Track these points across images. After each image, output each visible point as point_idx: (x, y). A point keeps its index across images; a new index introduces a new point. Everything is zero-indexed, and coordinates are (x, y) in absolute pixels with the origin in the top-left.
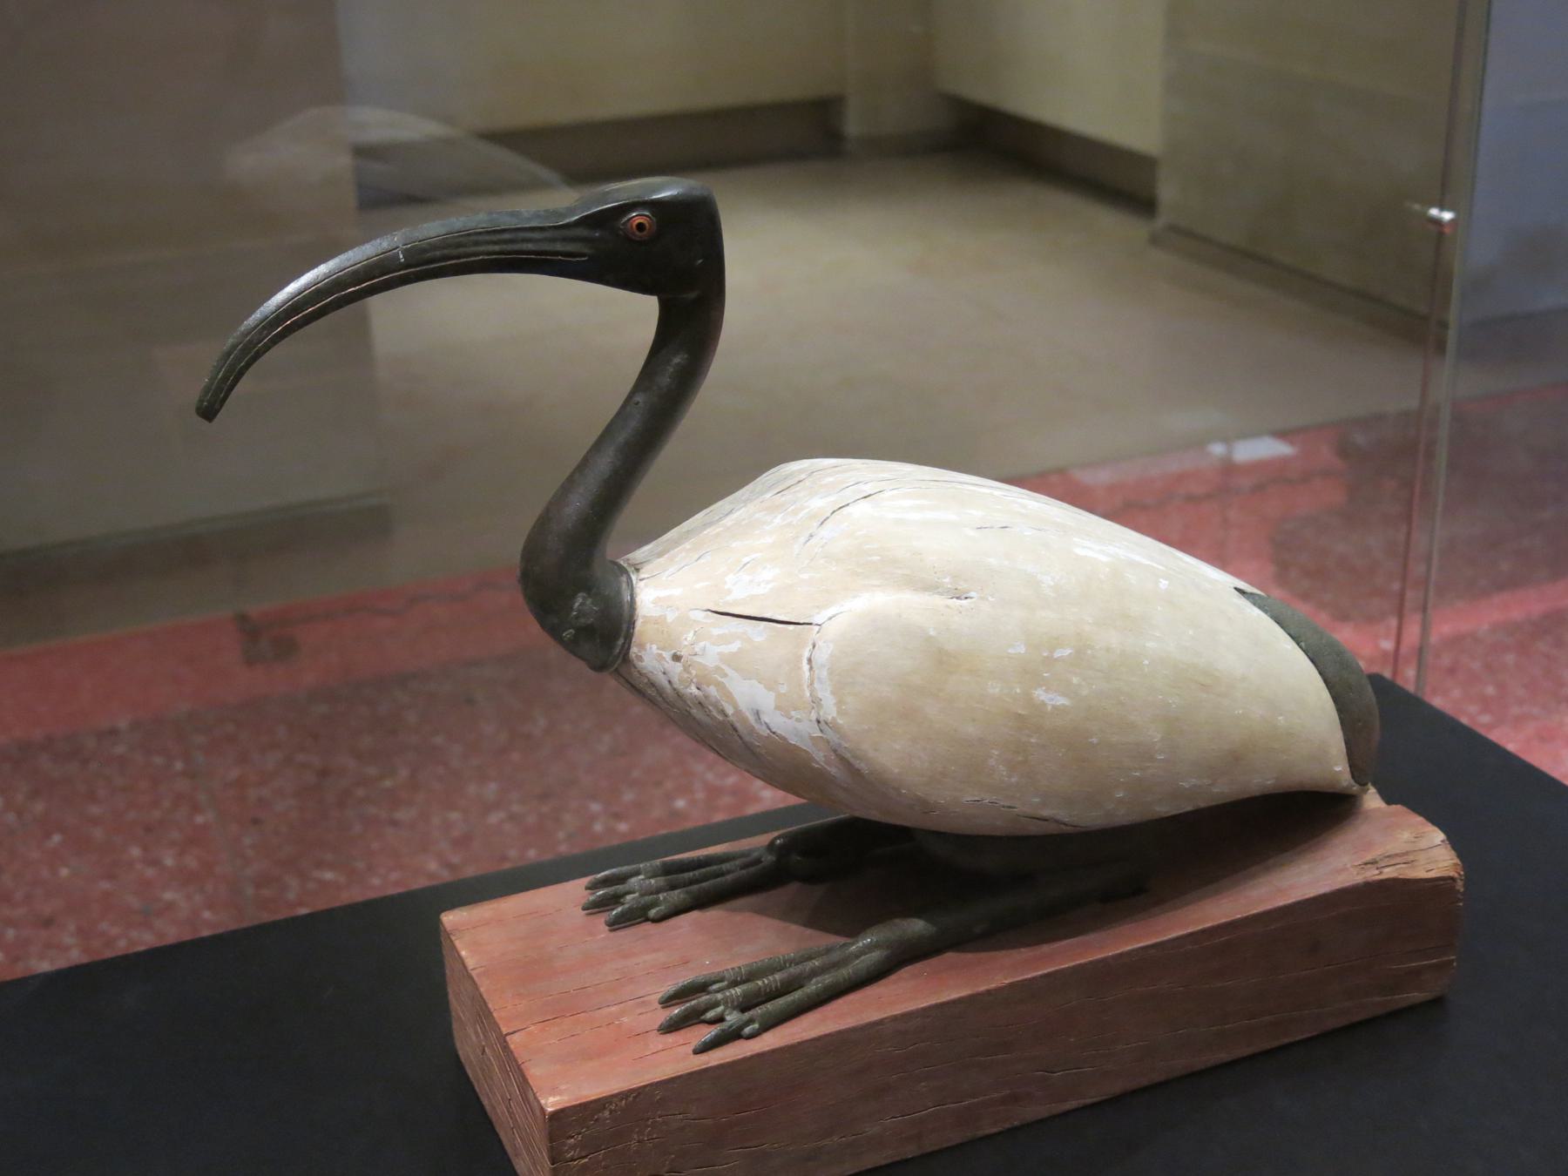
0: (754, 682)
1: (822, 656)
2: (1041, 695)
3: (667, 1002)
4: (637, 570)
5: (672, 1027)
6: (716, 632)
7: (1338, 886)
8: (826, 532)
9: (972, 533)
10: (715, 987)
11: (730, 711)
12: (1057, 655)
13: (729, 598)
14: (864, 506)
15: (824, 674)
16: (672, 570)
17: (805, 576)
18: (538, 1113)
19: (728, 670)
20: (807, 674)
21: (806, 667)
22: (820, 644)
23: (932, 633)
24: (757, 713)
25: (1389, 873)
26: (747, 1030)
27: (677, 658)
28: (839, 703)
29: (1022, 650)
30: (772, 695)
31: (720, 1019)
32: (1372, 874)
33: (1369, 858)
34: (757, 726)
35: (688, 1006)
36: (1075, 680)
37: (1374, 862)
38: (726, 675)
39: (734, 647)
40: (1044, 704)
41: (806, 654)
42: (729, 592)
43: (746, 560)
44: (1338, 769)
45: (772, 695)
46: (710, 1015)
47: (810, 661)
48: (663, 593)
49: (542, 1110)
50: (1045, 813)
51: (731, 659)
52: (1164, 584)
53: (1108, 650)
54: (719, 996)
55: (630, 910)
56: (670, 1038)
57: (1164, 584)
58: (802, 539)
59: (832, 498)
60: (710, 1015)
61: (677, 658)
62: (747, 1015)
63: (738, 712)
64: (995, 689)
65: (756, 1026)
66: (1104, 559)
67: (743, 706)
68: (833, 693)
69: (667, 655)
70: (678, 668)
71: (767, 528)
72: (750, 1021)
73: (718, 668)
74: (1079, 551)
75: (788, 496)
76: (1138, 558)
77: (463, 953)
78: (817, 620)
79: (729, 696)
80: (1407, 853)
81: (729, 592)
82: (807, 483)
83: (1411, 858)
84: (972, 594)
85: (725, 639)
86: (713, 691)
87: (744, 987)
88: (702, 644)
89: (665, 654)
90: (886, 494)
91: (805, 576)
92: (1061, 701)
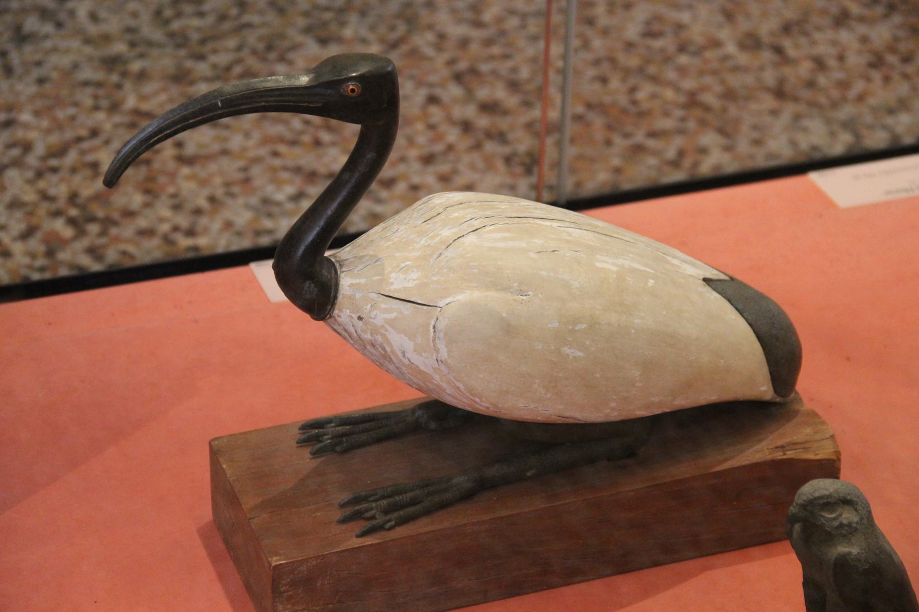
0: (403, 336)
1: (441, 325)
2: (566, 350)
3: (343, 506)
4: (341, 266)
5: (344, 521)
6: (383, 306)
7: (755, 461)
8: (449, 253)
9: (533, 255)
10: (372, 499)
11: (388, 349)
12: (578, 328)
13: (392, 288)
14: (472, 239)
15: (442, 335)
16: (360, 267)
17: (435, 279)
18: (266, 564)
19: (388, 328)
20: (432, 334)
21: (432, 330)
22: (440, 318)
23: (504, 315)
24: (404, 353)
25: (790, 454)
26: (388, 526)
27: (360, 318)
28: (449, 352)
29: (556, 325)
30: (412, 344)
31: (373, 518)
32: (779, 455)
33: (779, 443)
34: (403, 359)
35: (355, 512)
36: (587, 342)
37: (782, 447)
38: (387, 330)
39: (393, 315)
40: (568, 355)
41: (433, 323)
42: (392, 284)
43: (403, 265)
44: (763, 388)
45: (412, 344)
46: (367, 515)
47: (434, 327)
48: (355, 281)
49: (270, 564)
50: (567, 414)
51: (392, 323)
52: (651, 282)
53: (609, 324)
54: (374, 505)
55: (326, 446)
56: (343, 527)
57: (651, 282)
58: (435, 256)
59: (454, 230)
60: (367, 515)
61: (360, 318)
62: (388, 517)
63: (393, 352)
64: (539, 346)
65: (393, 523)
66: (615, 269)
67: (396, 348)
68: (446, 346)
69: (355, 316)
70: (360, 323)
71: (416, 246)
72: (389, 521)
73: (383, 326)
74: (599, 265)
75: (430, 224)
76: (637, 266)
77: (224, 466)
78: (441, 304)
79: (388, 342)
80: (806, 442)
81: (392, 284)
82: (442, 216)
83: (807, 445)
84: (530, 293)
85: (387, 311)
86: (379, 338)
87: (391, 500)
88: (375, 312)
89: (354, 316)
90: (487, 228)
91: (435, 279)
92: (579, 354)
